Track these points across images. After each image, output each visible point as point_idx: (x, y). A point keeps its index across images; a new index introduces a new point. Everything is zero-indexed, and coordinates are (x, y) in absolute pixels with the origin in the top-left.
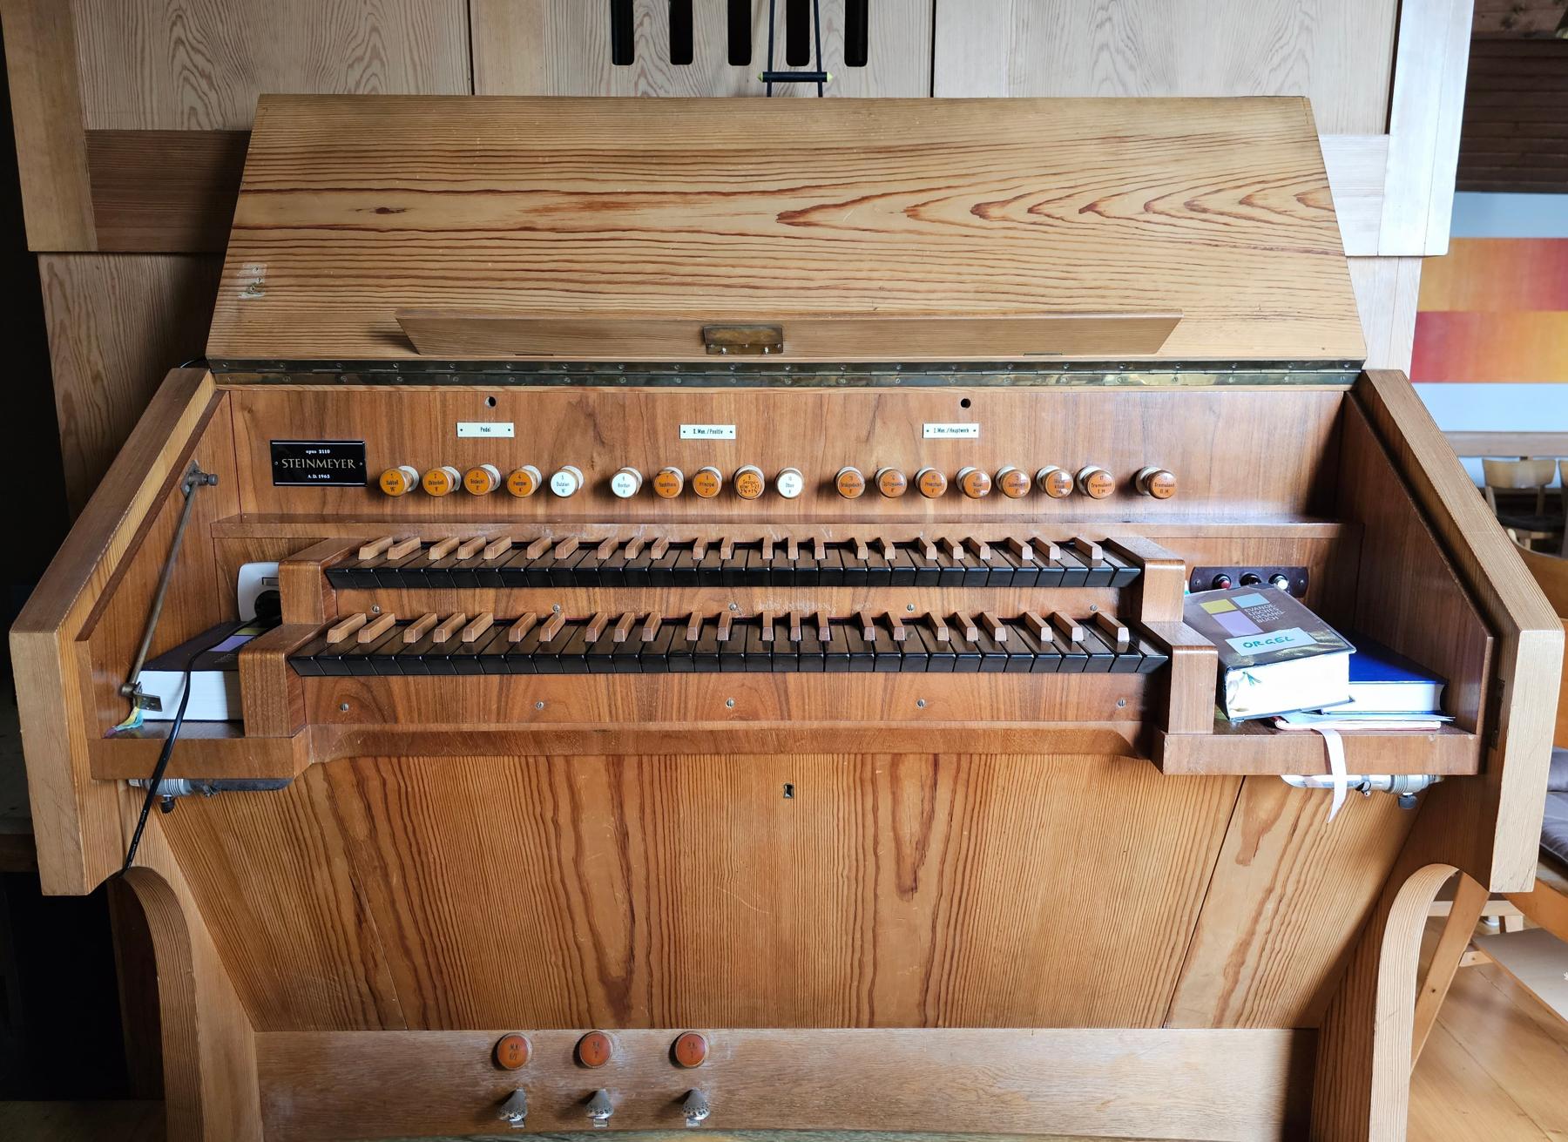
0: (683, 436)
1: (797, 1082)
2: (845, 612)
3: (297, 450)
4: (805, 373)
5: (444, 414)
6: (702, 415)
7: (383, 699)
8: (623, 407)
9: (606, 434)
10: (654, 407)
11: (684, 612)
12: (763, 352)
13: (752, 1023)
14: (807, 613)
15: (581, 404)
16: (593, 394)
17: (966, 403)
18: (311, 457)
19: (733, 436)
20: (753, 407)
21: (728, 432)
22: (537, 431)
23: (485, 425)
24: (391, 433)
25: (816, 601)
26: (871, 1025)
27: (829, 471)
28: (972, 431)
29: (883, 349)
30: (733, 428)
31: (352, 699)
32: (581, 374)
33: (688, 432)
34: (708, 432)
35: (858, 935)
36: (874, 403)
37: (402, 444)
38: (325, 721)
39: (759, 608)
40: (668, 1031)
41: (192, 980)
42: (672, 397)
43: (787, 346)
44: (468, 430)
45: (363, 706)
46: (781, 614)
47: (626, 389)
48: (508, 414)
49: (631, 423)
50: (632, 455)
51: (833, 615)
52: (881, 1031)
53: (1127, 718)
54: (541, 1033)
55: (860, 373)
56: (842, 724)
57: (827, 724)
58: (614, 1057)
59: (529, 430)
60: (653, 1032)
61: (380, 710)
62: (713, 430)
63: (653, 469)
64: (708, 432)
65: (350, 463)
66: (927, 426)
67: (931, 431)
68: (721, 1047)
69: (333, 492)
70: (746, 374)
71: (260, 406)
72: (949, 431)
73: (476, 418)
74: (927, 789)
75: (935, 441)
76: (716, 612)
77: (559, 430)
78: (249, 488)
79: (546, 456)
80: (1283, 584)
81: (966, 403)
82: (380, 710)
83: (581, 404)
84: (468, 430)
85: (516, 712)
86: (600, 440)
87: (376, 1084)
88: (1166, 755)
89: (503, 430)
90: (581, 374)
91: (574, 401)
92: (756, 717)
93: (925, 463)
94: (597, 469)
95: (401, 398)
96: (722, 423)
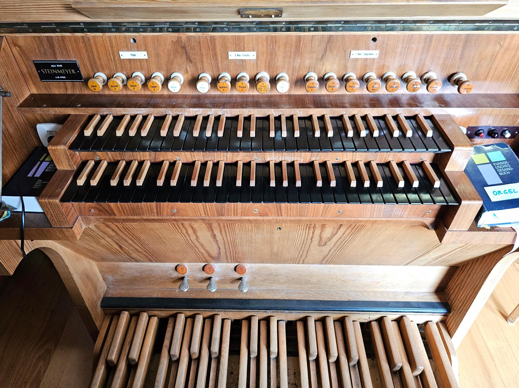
0: (230, 58)
1: (277, 276)
2: (307, 161)
3: (47, 65)
4: (293, 26)
5: (112, 47)
6: (239, 47)
7: (107, 208)
8: (199, 43)
9: (192, 57)
10: (215, 42)
11: (234, 160)
12: (271, 17)
13: (262, 262)
14: (290, 161)
15: (179, 40)
16: (184, 35)
17: (374, 40)
18: (54, 68)
19: (255, 58)
20: (265, 43)
21: (251, 56)
22: (158, 55)
23: (133, 53)
24: (89, 56)
25: (294, 157)
26: (303, 263)
27: (302, 74)
28: (375, 54)
29: (337, 15)
30: (255, 53)
31: (94, 208)
32: (176, 27)
33: (233, 55)
34: (242, 55)
35: (301, 252)
36: (326, 40)
37: (95, 63)
38: (85, 215)
39: (268, 159)
40: (234, 264)
41: (67, 266)
42: (224, 37)
43: (283, 15)
44: (125, 55)
45: (99, 210)
46: (278, 161)
47: (200, 34)
48: (143, 47)
49: (204, 51)
50: (205, 67)
51: (302, 162)
52: (306, 265)
53: (430, 217)
54: (191, 264)
55: (321, 26)
56: (304, 218)
57: (298, 218)
58: (215, 269)
59: (154, 54)
60: (228, 264)
61: (107, 212)
62: (245, 55)
63: (216, 74)
64: (242, 55)
65: (73, 71)
66: (353, 52)
67: (355, 54)
68: (251, 268)
69: (69, 84)
70: (262, 27)
71: (21, 42)
72: (364, 54)
73: (128, 49)
74: (336, 230)
75: (356, 60)
76: (248, 160)
77: (169, 55)
78: (30, 82)
79: (164, 67)
80: (508, 135)
81: (374, 40)
82: (107, 212)
83: (179, 40)
84: (125, 55)
85: (165, 213)
86: (189, 60)
87: (138, 274)
88: (445, 238)
89: (142, 55)
90: (176, 27)
91: (174, 40)
92: (267, 215)
93: (349, 70)
94: (189, 73)
95: (89, 39)
96: (249, 51)
